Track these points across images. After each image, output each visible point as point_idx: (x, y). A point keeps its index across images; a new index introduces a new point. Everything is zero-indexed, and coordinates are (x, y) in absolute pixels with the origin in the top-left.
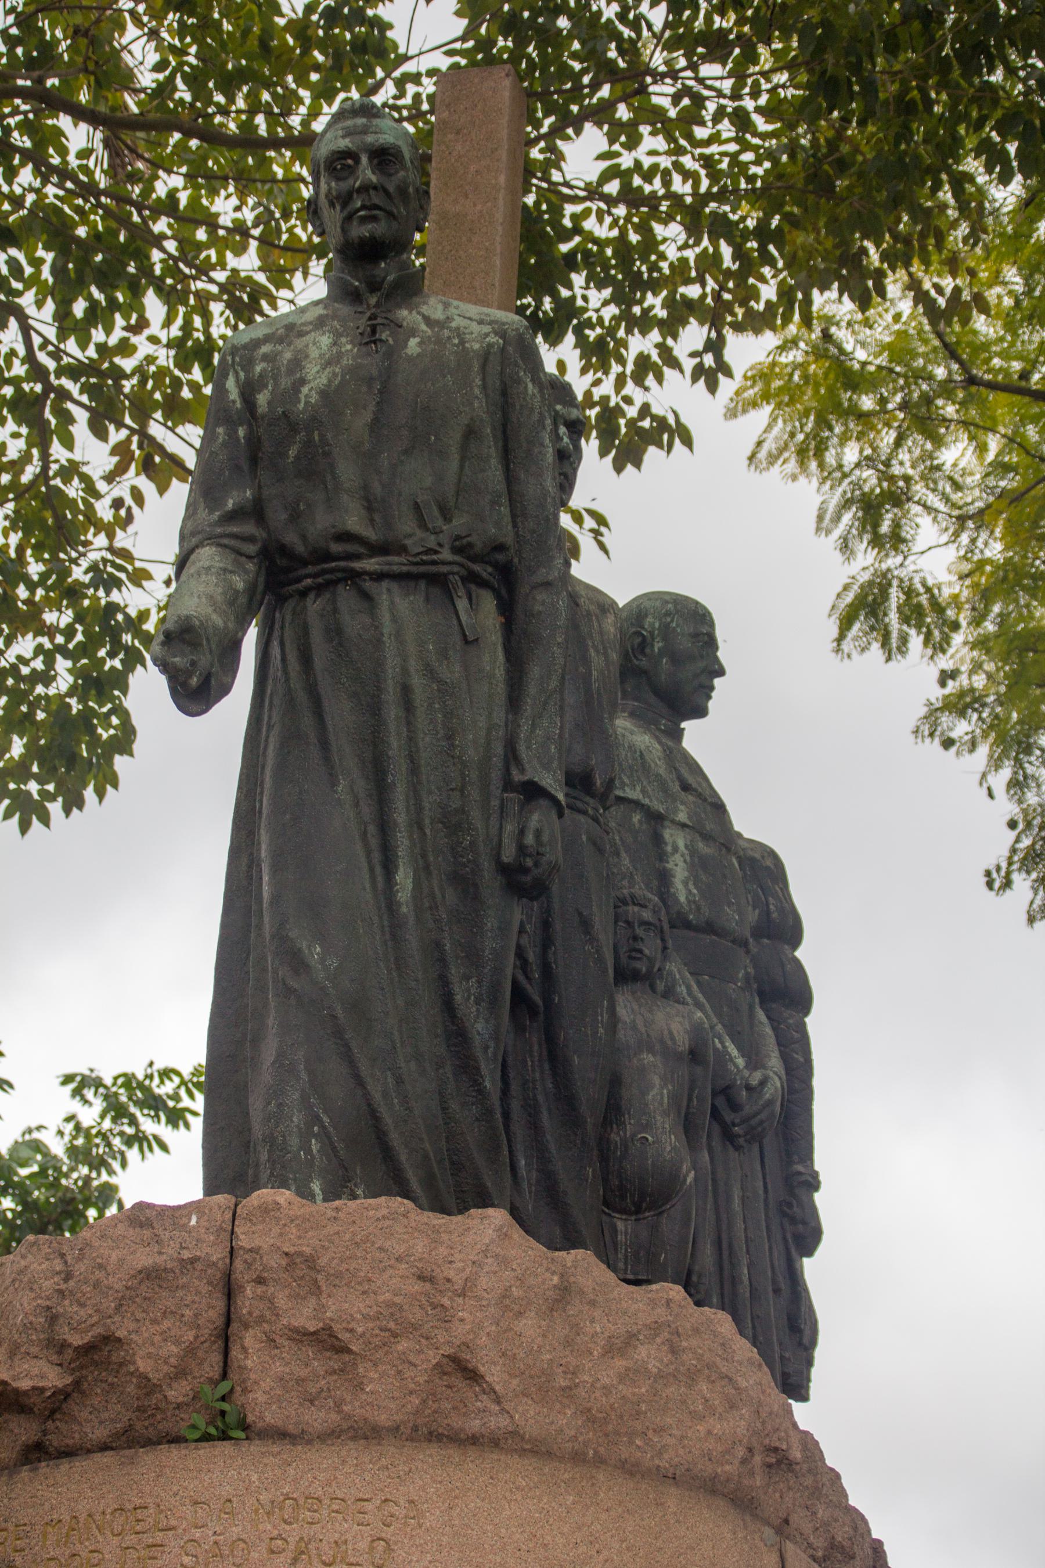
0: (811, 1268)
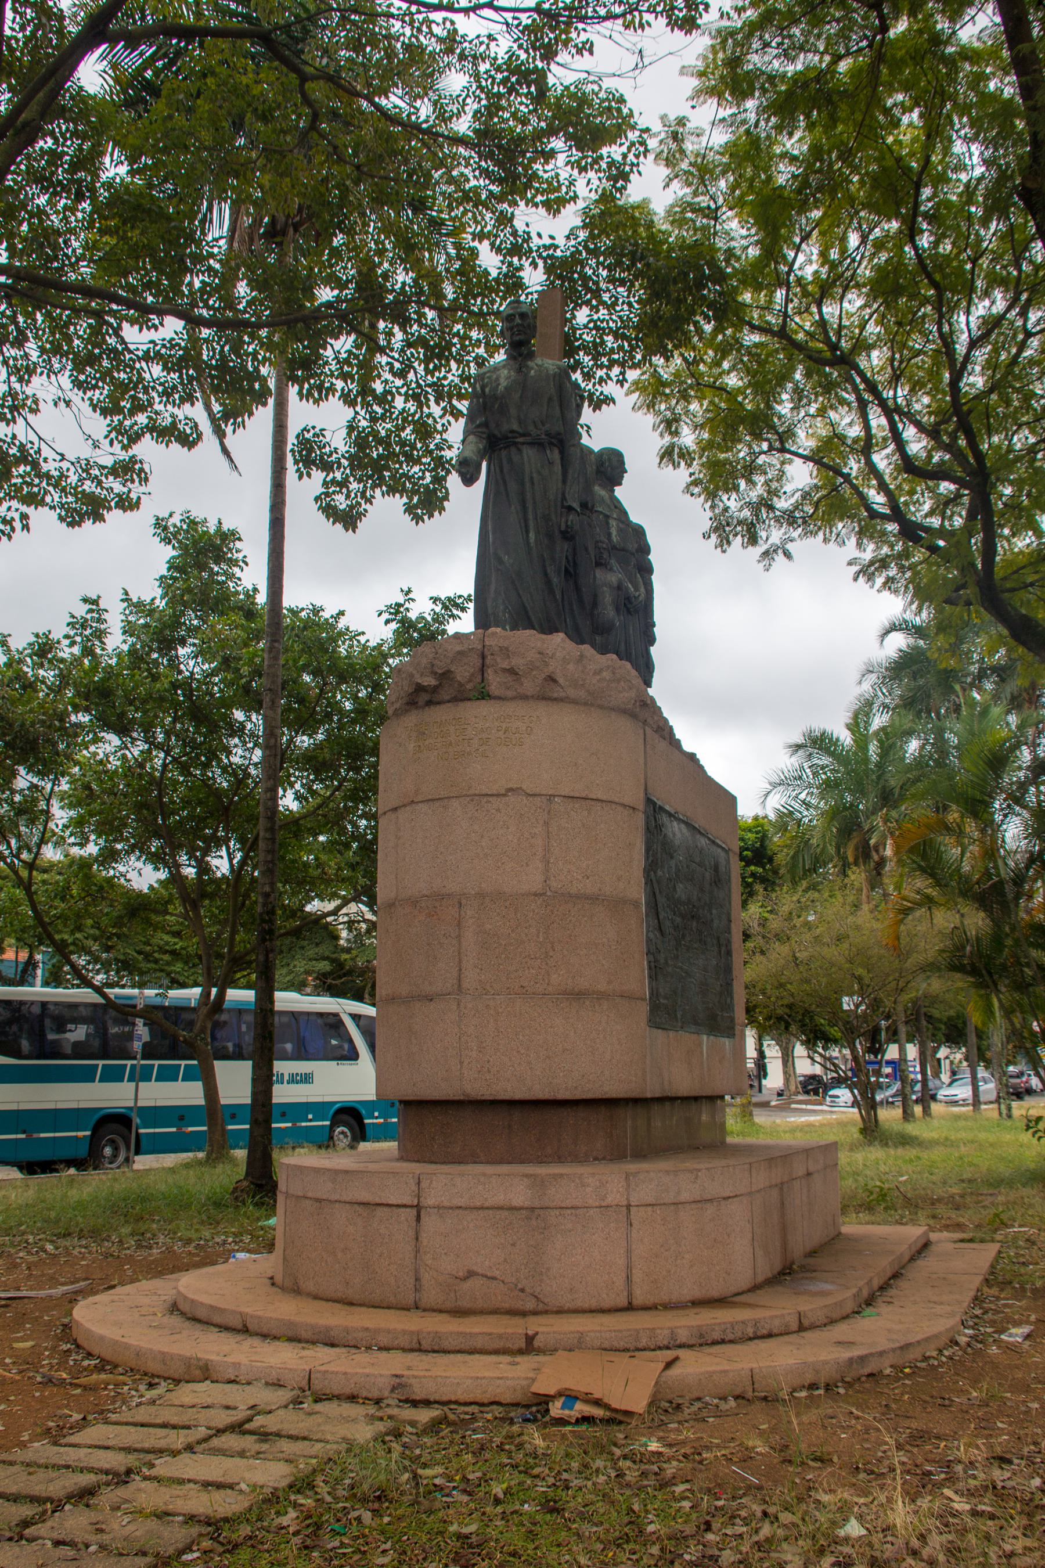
0: (653, 650)
